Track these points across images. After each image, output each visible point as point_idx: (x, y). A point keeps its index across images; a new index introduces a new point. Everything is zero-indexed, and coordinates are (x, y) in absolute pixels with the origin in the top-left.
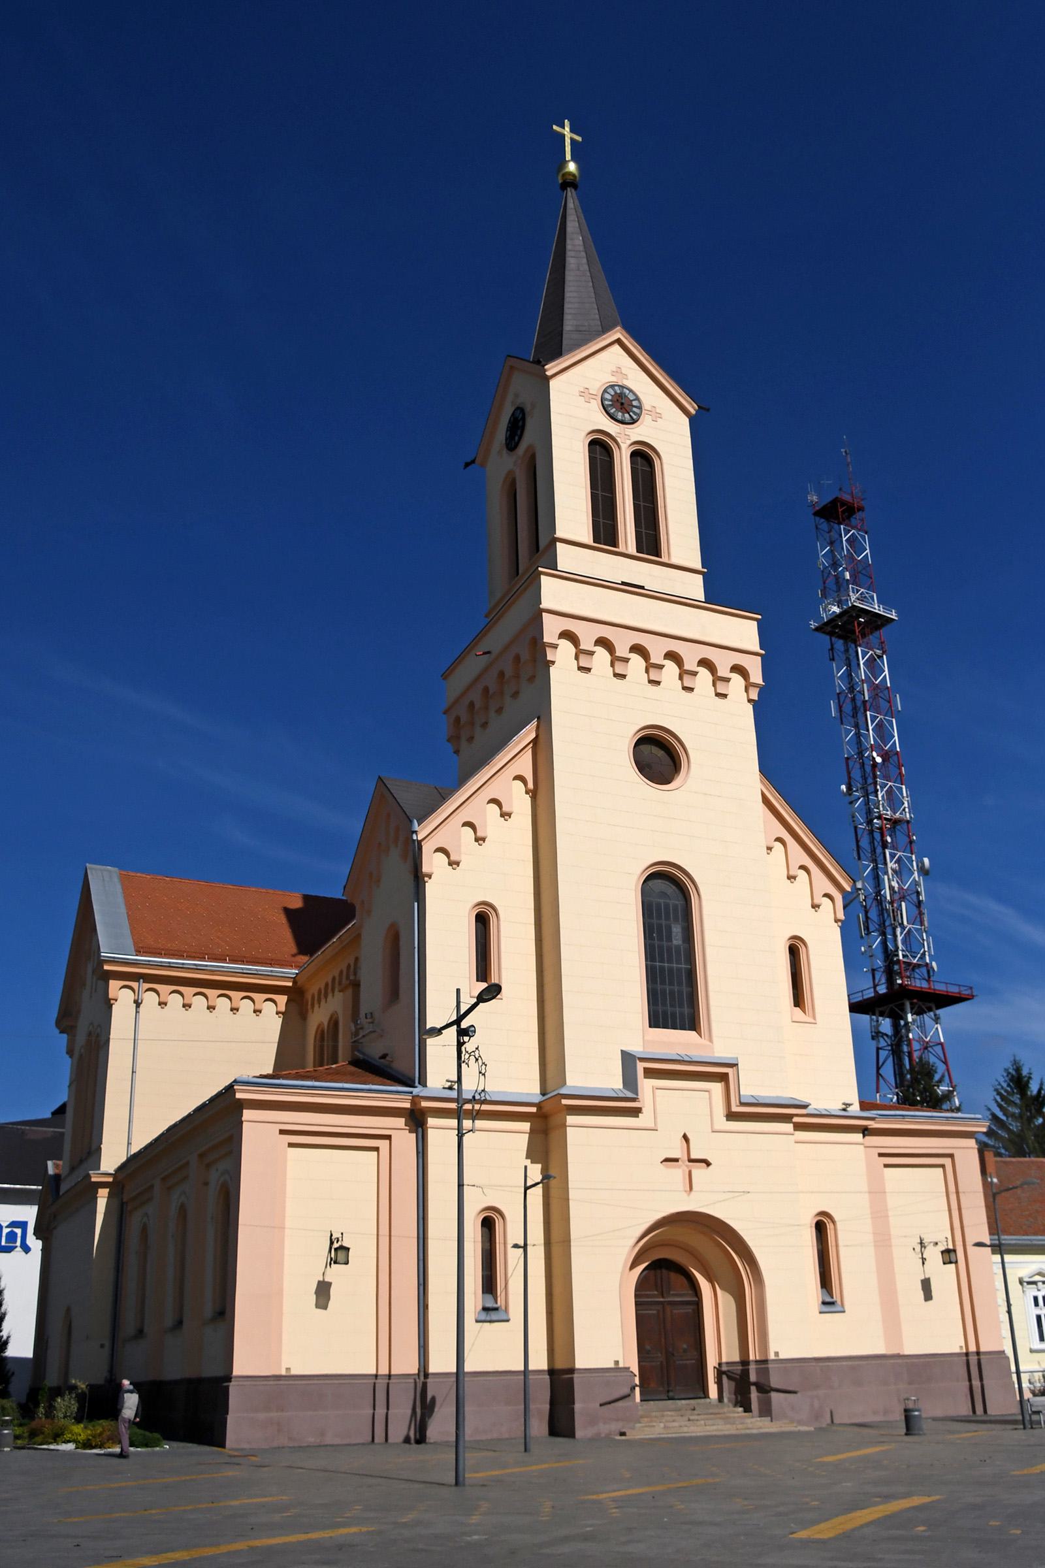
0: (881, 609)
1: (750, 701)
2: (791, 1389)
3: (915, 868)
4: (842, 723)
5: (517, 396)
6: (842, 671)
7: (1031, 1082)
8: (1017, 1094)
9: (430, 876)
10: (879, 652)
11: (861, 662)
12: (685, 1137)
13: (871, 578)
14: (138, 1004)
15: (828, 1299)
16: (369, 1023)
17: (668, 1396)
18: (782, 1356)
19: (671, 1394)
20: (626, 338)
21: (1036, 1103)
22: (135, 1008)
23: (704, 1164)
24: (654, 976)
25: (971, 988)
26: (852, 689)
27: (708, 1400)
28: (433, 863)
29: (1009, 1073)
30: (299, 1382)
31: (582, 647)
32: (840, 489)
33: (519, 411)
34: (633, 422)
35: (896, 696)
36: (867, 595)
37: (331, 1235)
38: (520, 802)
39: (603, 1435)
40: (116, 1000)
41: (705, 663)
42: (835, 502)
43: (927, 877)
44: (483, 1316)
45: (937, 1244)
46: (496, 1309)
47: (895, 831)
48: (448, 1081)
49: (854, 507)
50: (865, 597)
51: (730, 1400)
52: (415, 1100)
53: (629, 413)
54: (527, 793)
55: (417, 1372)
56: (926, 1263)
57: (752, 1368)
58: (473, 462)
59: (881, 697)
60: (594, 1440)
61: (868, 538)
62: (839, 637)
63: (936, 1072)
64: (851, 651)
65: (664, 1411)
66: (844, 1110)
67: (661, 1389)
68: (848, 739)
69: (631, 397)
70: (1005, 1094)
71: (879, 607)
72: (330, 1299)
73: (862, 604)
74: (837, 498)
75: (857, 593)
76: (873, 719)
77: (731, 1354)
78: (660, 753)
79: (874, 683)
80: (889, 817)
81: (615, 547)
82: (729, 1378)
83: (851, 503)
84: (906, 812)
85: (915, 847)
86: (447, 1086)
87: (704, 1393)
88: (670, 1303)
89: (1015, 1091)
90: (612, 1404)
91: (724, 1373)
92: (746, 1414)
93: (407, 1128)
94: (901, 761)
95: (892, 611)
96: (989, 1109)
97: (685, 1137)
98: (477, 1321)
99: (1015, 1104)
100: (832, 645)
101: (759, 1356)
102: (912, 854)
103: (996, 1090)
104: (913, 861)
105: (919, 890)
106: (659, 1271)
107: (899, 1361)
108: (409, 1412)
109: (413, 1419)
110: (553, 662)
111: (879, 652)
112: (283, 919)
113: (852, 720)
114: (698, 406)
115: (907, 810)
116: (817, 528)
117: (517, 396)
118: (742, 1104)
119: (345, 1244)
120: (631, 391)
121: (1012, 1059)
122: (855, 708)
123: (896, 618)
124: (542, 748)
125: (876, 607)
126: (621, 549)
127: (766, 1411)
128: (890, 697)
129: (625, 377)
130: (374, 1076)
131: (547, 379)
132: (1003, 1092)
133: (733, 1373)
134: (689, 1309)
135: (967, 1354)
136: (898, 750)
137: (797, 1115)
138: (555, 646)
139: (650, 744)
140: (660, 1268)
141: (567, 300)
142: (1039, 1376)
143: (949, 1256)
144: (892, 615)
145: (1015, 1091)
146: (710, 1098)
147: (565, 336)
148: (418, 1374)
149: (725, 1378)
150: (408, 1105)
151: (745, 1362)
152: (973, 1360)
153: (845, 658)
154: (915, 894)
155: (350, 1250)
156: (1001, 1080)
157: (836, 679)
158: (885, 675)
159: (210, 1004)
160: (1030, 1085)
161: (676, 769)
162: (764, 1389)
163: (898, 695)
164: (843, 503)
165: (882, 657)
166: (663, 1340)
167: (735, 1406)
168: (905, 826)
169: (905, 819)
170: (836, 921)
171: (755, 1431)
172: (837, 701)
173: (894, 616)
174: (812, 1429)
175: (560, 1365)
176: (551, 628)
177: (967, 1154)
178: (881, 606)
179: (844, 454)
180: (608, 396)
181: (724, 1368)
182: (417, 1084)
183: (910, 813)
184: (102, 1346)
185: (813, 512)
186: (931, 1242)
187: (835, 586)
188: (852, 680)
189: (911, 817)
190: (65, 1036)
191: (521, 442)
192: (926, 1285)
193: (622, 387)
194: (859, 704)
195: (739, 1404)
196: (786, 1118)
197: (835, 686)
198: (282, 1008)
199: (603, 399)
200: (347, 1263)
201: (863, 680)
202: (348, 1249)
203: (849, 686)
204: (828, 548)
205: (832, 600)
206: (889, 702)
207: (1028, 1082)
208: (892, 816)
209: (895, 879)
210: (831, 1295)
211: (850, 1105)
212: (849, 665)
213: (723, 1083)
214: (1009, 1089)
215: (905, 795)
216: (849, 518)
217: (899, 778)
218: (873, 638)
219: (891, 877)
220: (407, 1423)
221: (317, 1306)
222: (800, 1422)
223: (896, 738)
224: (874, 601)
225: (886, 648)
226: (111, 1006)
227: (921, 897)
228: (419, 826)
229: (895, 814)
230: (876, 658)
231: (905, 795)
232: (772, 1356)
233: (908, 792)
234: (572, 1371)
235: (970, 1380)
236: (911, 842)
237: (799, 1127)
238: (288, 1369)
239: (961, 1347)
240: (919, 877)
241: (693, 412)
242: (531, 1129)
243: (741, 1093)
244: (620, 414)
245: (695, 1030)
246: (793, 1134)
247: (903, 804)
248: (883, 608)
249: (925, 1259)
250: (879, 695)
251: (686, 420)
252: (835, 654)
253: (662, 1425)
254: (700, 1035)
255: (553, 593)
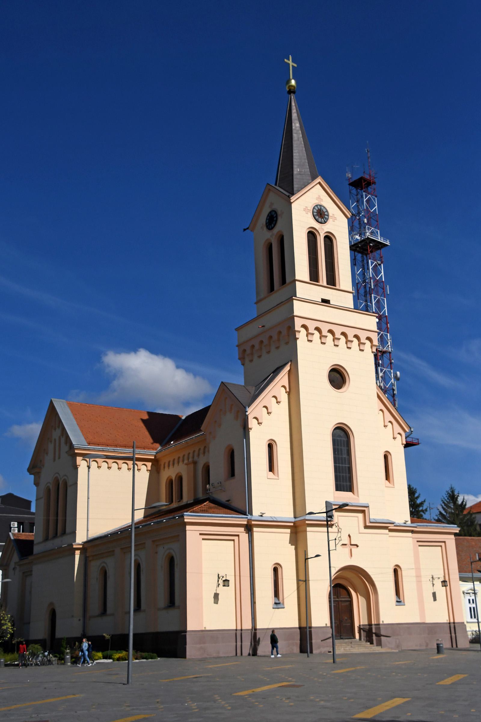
0: (382, 239)
1: (372, 352)
2: (388, 635)
3: (393, 377)
4: (358, 299)
5: (272, 204)
6: (360, 271)
7: (458, 498)
8: (452, 503)
9: (251, 429)
10: (379, 262)
11: (371, 268)
12: (349, 536)
13: (377, 222)
14: (89, 467)
15: (399, 600)
16: (219, 486)
17: (341, 638)
18: (385, 623)
19: (342, 637)
20: (322, 182)
21: (460, 507)
22: (87, 469)
23: (356, 546)
24: (337, 470)
25: (418, 439)
26: (364, 281)
27: (355, 640)
28: (252, 423)
29: (448, 493)
30: (209, 633)
31: (309, 332)
32: (364, 172)
33: (274, 213)
34: (325, 222)
35: (387, 286)
36: (375, 231)
37: (218, 575)
38: (284, 397)
39: (322, 652)
40: (80, 466)
41: (356, 336)
42: (361, 179)
43: (398, 381)
44: (275, 606)
45: (439, 578)
46: (279, 603)
47: (383, 357)
48: (261, 513)
49: (371, 182)
50: (374, 232)
51: (364, 640)
52: (249, 521)
53: (323, 218)
54: (286, 392)
55: (251, 628)
56: (434, 586)
57: (373, 627)
58: (248, 229)
59: (379, 286)
60: (320, 654)
61: (377, 200)
62: (359, 252)
63: (416, 492)
64: (365, 261)
65: (342, 643)
66: (405, 523)
67: (338, 635)
68: (361, 307)
69: (324, 210)
70: (447, 503)
71: (381, 238)
72: (218, 600)
73: (372, 237)
74: (362, 177)
75: (370, 230)
76: (375, 298)
77: (364, 621)
78: (338, 375)
79: (376, 279)
80: (380, 350)
81: (318, 282)
82: (363, 631)
83: (369, 180)
84: (389, 348)
85: (393, 366)
86: (260, 515)
87: (353, 636)
88: (341, 601)
89: (451, 502)
90: (326, 641)
91: (362, 629)
92: (371, 645)
93: (245, 532)
94: (388, 321)
95: (387, 241)
96: (438, 509)
97: (349, 536)
98: (273, 608)
99: (451, 508)
100: (355, 257)
101: (376, 622)
102: (391, 369)
103: (442, 501)
104: (391, 373)
105: (394, 388)
106: (336, 588)
107: (425, 625)
108: (250, 644)
109: (251, 647)
110: (298, 338)
111: (379, 262)
112: (142, 424)
113: (364, 298)
114: (351, 213)
115: (390, 346)
116: (350, 192)
117: (272, 204)
118: (371, 522)
119: (227, 579)
120: (324, 207)
121: (450, 487)
122: (366, 292)
123: (389, 245)
124: (294, 376)
125: (379, 238)
126: (320, 283)
127: (379, 644)
128: (384, 286)
129: (321, 200)
130: (224, 509)
131: (291, 203)
132: (445, 502)
133: (365, 629)
134: (348, 603)
135: (450, 623)
136: (387, 315)
137: (392, 526)
138: (299, 332)
139: (334, 372)
140: (337, 587)
141: (294, 157)
142: (470, 633)
143: (444, 583)
144: (387, 243)
145: (451, 502)
146: (358, 520)
147: (295, 177)
148: (252, 629)
149: (362, 631)
150: (246, 523)
151: (370, 625)
152: (452, 625)
153: (362, 265)
154: (392, 390)
155: (230, 581)
156: (445, 496)
157: (356, 275)
158: (382, 275)
159: (109, 466)
160: (458, 499)
161: (343, 381)
162: (378, 635)
163: (388, 286)
164: (365, 180)
165: (381, 265)
166: (338, 616)
167: (366, 641)
168: (388, 354)
169: (388, 351)
170: (402, 444)
171: (377, 652)
172: (356, 287)
173: (388, 243)
174: (397, 651)
175: (304, 625)
176: (298, 323)
177: (451, 541)
178: (382, 238)
179: (366, 151)
180: (315, 211)
181: (362, 627)
182: (247, 514)
183: (391, 348)
184: (80, 620)
185: (348, 183)
186: (437, 577)
187: (358, 225)
188: (365, 277)
189: (392, 350)
190: (32, 476)
191: (275, 227)
192: (434, 594)
193: (321, 206)
194: (368, 289)
195: (368, 641)
196: (386, 528)
197: (356, 279)
198: (149, 468)
199: (313, 212)
200: (228, 586)
201: (370, 277)
202: (229, 581)
203: (363, 280)
204: (355, 203)
205: (356, 232)
206: (383, 289)
207: (457, 498)
208: (382, 350)
209: (382, 383)
210: (399, 598)
211: (407, 521)
212: (364, 268)
213: (363, 514)
214: (448, 500)
215: (389, 338)
216: (367, 187)
217: (386, 330)
218: (377, 253)
219: (380, 381)
220: (249, 648)
221: (215, 603)
222: (392, 648)
223: (386, 308)
224: (378, 235)
225: (383, 260)
226: (77, 468)
227: (395, 392)
228: (248, 408)
229: (383, 349)
230: (377, 265)
231: (389, 338)
232: (381, 623)
233: (391, 337)
234: (310, 627)
235: (451, 634)
236: (391, 363)
237: (391, 530)
238: (205, 628)
239: (447, 620)
240: (394, 382)
241: (349, 216)
242: (291, 532)
243: (370, 518)
244: (320, 219)
245: (351, 492)
246: (388, 534)
247: (388, 343)
248: (383, 239)
249: (434, 584)
250: (378, 285)
251: (346, 220)
252: (356, 262)
253: (343, 649)
254: (354, 494)
255: (299, 308)
